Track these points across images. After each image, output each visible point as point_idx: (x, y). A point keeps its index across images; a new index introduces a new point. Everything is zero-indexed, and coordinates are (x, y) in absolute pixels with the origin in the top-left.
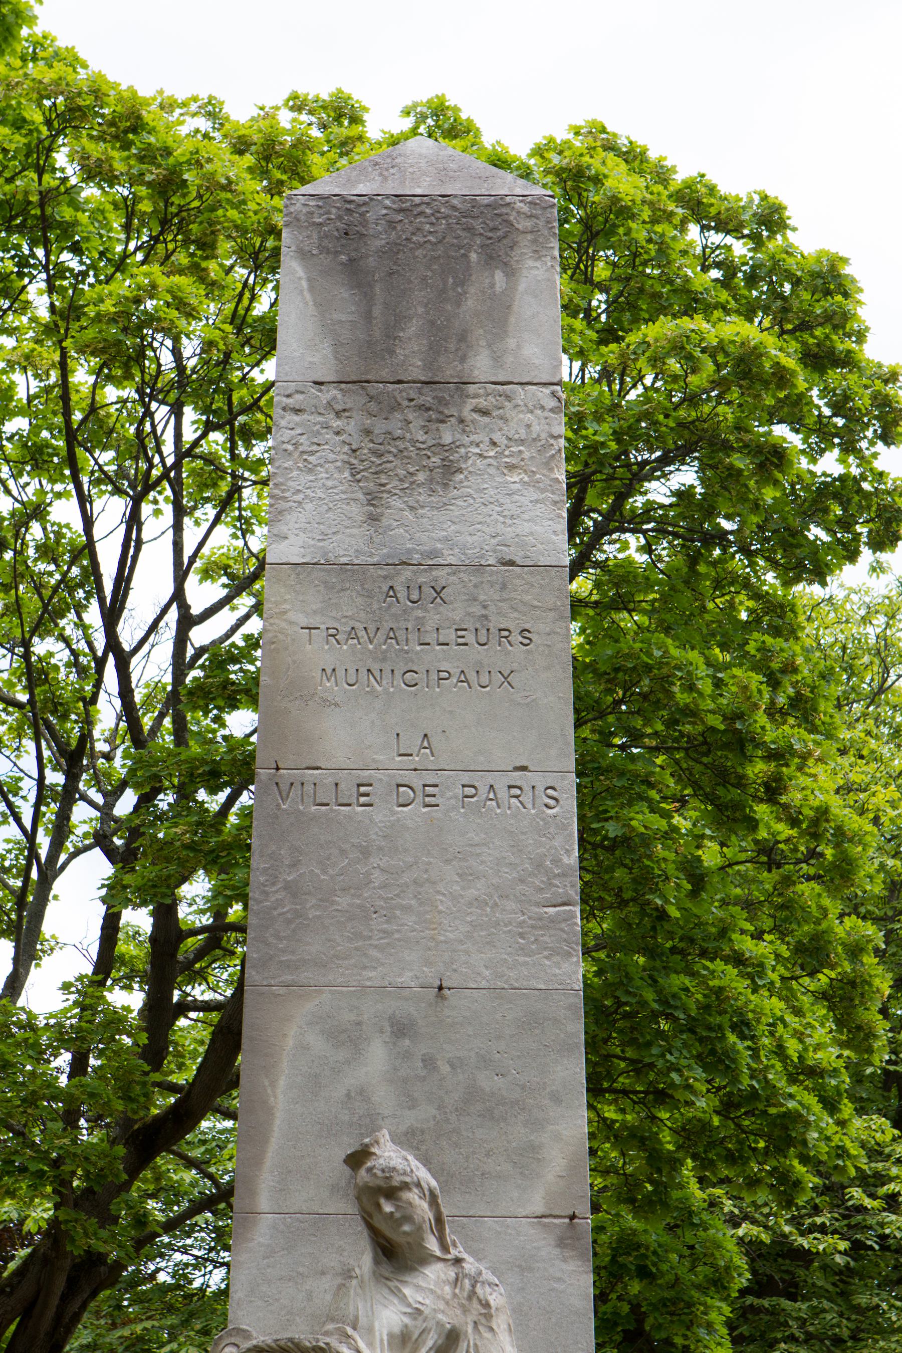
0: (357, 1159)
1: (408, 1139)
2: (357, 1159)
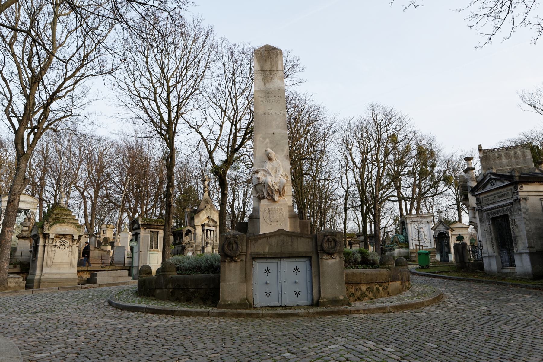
0: (266, 151)
1: (271, 148)
2: (266, 151)
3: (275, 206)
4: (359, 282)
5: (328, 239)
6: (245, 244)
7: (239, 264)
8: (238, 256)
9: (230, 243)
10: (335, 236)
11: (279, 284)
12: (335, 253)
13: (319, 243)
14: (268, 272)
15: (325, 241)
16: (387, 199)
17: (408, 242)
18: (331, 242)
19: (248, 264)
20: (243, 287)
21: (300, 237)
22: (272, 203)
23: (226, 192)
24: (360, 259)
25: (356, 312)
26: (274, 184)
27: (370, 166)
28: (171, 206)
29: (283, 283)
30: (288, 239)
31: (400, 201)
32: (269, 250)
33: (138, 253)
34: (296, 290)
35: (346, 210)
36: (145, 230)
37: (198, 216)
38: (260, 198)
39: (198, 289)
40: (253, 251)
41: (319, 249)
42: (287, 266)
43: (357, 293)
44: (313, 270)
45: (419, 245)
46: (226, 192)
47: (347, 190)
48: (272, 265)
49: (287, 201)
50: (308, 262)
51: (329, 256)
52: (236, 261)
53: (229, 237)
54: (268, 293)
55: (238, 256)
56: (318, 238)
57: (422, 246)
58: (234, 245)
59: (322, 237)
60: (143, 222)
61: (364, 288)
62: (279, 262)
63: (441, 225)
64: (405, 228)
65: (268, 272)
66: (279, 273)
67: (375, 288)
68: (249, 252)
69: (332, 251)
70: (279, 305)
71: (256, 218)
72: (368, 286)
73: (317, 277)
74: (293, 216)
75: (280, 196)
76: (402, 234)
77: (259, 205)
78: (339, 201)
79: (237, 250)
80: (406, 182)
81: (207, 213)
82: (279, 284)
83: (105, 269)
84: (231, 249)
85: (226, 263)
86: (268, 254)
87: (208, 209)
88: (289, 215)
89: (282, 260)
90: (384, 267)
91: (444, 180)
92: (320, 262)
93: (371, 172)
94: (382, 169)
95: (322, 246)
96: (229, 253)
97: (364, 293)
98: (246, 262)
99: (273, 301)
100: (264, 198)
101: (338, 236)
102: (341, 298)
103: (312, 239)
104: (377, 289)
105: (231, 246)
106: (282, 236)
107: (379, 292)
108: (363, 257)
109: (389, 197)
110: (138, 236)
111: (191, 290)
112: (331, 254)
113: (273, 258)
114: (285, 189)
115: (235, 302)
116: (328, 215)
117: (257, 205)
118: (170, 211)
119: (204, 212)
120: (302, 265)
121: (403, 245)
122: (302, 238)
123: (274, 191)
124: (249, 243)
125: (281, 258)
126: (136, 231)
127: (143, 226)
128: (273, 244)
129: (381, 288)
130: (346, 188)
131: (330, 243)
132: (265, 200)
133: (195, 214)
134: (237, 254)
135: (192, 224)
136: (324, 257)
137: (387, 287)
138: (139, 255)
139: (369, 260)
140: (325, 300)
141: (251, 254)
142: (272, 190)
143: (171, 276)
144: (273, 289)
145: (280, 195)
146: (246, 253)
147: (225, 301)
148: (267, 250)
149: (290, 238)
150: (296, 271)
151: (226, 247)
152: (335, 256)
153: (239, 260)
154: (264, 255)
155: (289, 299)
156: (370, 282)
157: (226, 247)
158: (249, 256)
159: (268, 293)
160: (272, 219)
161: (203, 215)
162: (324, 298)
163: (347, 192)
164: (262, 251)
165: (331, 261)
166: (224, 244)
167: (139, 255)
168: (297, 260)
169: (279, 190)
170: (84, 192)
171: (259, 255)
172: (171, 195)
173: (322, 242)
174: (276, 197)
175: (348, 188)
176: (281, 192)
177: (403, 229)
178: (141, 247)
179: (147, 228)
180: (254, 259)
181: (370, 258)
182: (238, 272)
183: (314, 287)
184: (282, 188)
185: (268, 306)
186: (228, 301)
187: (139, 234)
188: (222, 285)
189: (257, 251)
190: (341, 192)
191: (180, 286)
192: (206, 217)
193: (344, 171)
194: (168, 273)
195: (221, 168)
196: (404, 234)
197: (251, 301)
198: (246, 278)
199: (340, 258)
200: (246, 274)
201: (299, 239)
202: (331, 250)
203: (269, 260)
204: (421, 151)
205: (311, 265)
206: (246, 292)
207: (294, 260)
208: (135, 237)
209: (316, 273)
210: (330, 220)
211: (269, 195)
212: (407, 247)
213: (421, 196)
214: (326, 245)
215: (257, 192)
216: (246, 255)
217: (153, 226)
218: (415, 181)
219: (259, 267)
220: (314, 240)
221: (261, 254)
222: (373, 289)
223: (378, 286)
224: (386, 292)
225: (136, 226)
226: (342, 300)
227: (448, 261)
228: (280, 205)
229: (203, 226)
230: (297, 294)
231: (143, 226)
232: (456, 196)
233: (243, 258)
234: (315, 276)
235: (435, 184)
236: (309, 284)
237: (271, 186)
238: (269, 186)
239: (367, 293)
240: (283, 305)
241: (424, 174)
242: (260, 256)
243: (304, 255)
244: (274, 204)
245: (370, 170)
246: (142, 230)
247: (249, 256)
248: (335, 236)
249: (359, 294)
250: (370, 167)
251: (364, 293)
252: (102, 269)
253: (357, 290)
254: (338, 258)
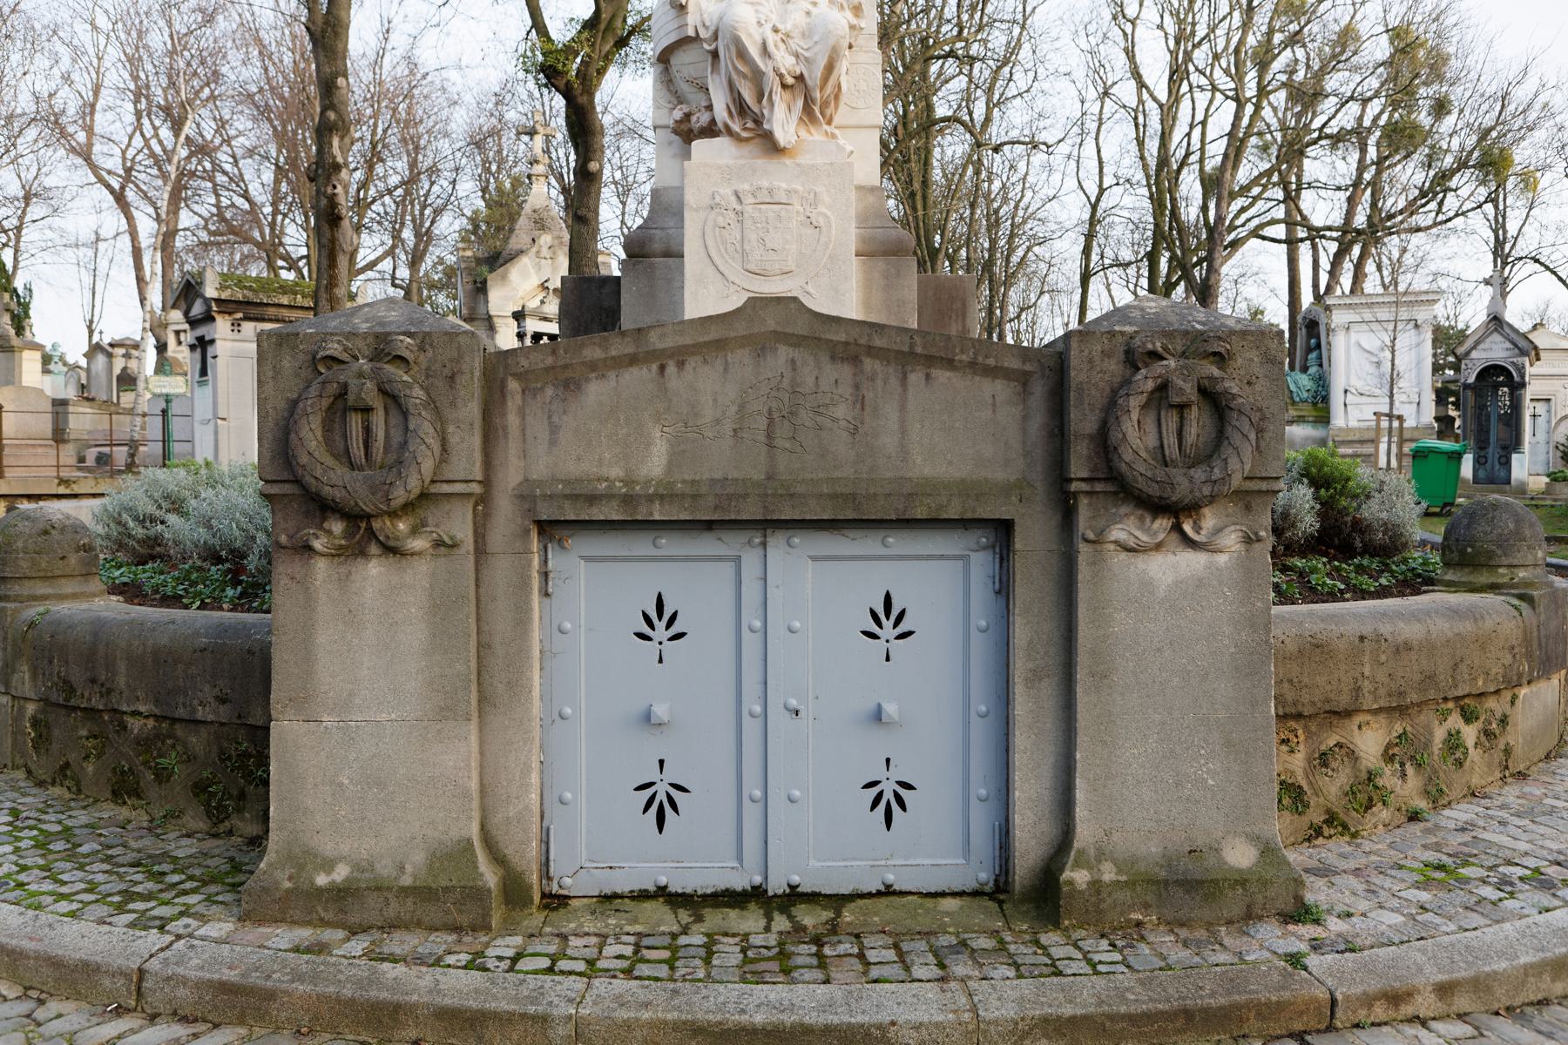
3: (776, 176)
4: (1344, 701)
5: (1163, 387)
6: (471, 409)
7: (419, 573)
8: (408, 507)
9: (341, 405)
10: (1220, 358)
11: (751, 728)
12: (1212, 499)
13: (1083, 421)
14: (661, 632)
15: (1135, 403)
16: (1255, 233)
17: (1326, 399)
18: (1182, 408)
19: (501, 570)
20: (458, 755)
21: (930, 361)
22: (761, 163)
23: (593, 166)
24: (1308, 523)
25: (1380, 1011)
26: (772, 39)
27: (1202, 99)
28: (340, 218)
29: (777, 716)
30: (834, 377)
31: (1291, 243)
32: (671, 465)
33: (211, 426)
34: (878, 773)
35: (1085, 278)
36: (236, 325)
37: (504, 277)
38: (686, 133)
39: (174, 720)
40: (541, 468)
41: (1078, 468)
42: (815, 590)
43: (1323, 781)
44: (1021, 633)
45: (1390, 416)
46: (593, 166)
47: (1098, 199)
48: (697, 580)
49: (846, 152)
50: (982, 565)
51: (1163, 524)
52: (392, 550)
53: (334, 348)
54: (662, 790)
55: (408, 507)
56: (1078, 373)
57: (1400, 418)
58: (378, 420)
59: (1114, 367)
60: (222, 288)
61: (1370, 741)
62: (751, 560)
63: (1496, 337)
64: (1318, 346)
65: (661, 632)
66: (751, 643)
67: (1439, 734)
68: (511, 475)
69: (1183, 485)
70: (740, 883)
71: (667, 254)
72: (1398, 728)
73: (1049, 689)
74: (876, 251)
75: (809, 114)
76: (1305, 369)
77: (683, 176)
78: (1058, 245)
79: (399, 461)
80: (1326, 168)
81: (539, 268)
82: (751, 728)
83: (76, 489)
84: (357, 451)
85: (321, 566)
86: (666, 495)
87: (545, 252)
88: (863, 240)
89: (778, 546)
90: (1484, 578)
91: (1480, 165)
92: (1084, 572)
93: (1204, 123)
94: (1249, 109)
95: (1104, 444)
96: (334, 478)
97: (1371, 776)
98: (481, 551)
99: (699, 857)
100: (710, 131)
101: (1247, 359)
102: (1240, 856)
103: (1023, 380)
104: (1453, 743)
105: (355, 422)
106: (784, 352)
107: (1459, 763)
108: (1327, 510)
109: (1262, 226)
110: (210, 351)
111: (135, 724)
112: (1173, 510)
113: (709, 526)
114: (843, 66)
115: (385, 869)
116: (1014, 296)
117: (670, 180)
118: (333, 241)
119: (525, 261)
120: (937, 584)
121: (1307, 410)
122: (942, 375)
123: (772, 82)
124: (514, 402)
125: (768, 525)
126: (200, 332)
127: (227, 306)
128: (709, 413)
129: (1470, 733)
130: (1093, 191)
131: (1171, 421)
132: (721, 142)
133: (492, 270)
134: (399, 496)
135: (481, 310)
136: (1117, 533)
137: (1504, 721)
138: (216, 433)
139: (1358, 526)
140: (1108, 874)
141: (526, 496)
142: (757, 77)
143: (32, 612)
144: (702, 765)
145: (808, 109)
146: (486, 482)
147: (306, 859)
148: (655, 464)
149: (846, 371)
150: (888, 630)
151: (311, 435)
152: (1209, 519)
153: (418, 544)
154: (628, 500)
155: (824, 845)
156: (1414, 697)
157: (311, 435)
158: (505, 510)
159: (662, 790)
160: (756, 257)
161: (525, 275)
162: (1101, 855)
163: (1094, 207)
164: (616, 472)
165: (1171, 567)
166: (293, 404)
167: (216, 433)
168: (897, 542)
169: (800, 78)
170: (123, 188)
171: (592, 499)
172: (337, 168)
173: (1111, 408)
174: (783, 121)
175: (1102, 191)
176: (814, 100)
177: (1309, 350)
178: (221, 399)
179: (247, 318)
180: (549, 529)
181: (1372, 511)
182: (414, 634)
183: (1018, 759)
184: (822, 63)
185: (662, 893)
186: (329, 865)
187: (212, 341)
188: (286, 732)
189: (572, 469)
190: (1073, 210)
191: (70, 689)
192: (535, 281)
193: (1089, 129)
194: (25, 589)
195: (569, 50)
196: (1313, 370)
197: (527, 858)
198: (484, 679)
199: (1249, 540)
200: (483, 647)
201: (916, 377)
202: (1178, 475)
203: (669, 544)
204: (1404, 42)
205: (1004, 589)
207: (867, 543)
208: (198, 354)
209: (1047, 657)
210: (1018, 317)
211: (741, 108)
212: (1324, 418)
213: (1374, 233)
214: (1138, 436)
215: (680, 100)
216: (483, 501)
217: (272, 311)
218: (1361, 168)
219: (590, 600)
220: (1039, 390)
221: (609, 496)
222: (1427, 745)
223: (1455, 721)
224: (1498, 756)
225: (197, 309)
226: (1241, 880)
227: (1508, 482)
229: (519, 316)
230: (889, 804)
231: (227, 306)
232: (1495, 232)
233: (459, 525)
234: (1034, 677)
235: (1439, 185)
236: (982, 735)
237: (754, 52)
238: (742, 53)
239: (1389, 778)
240: (776, 886)
241: (1401, 138)
242: (598, 513)
243: (952, 514)
245: (1199, 117)
246: (222, 326)
247: (505, 510)
248: (1220, 358)
249: (1334, 785)
250: (1202, 99)
251: (1371, 776)
252: (62, 490)
253: (1324, 759)
254: (1231, 539)
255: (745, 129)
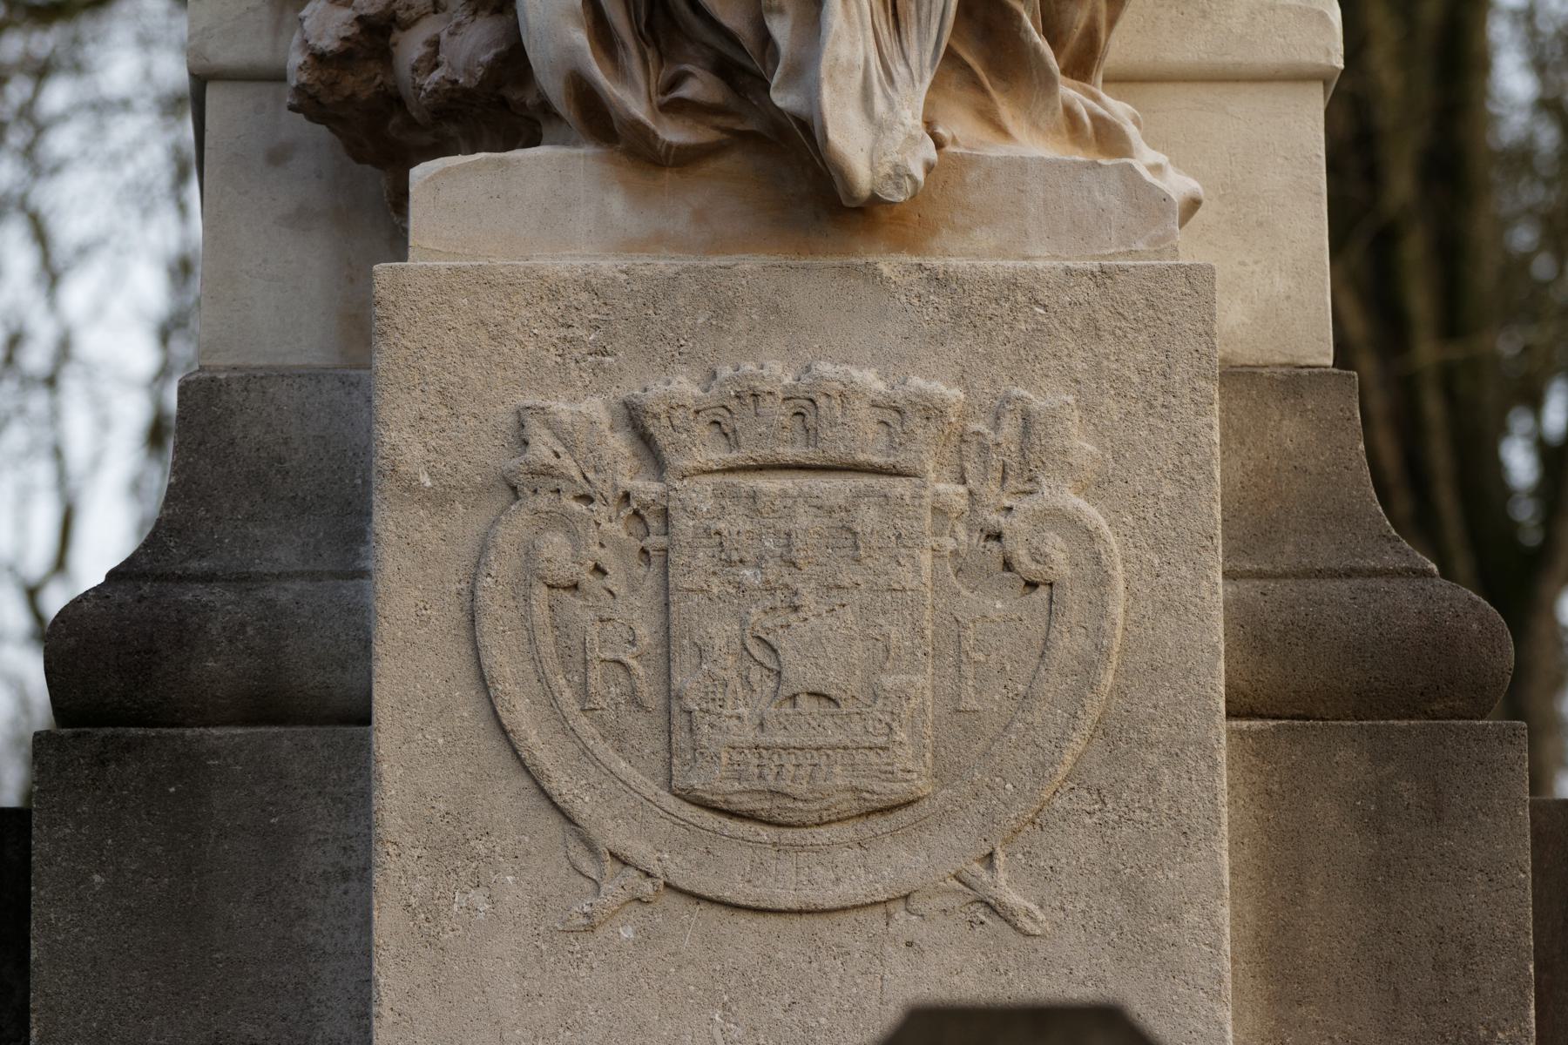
3: (848, 341)
77: (358, 324)
100: (500, 109)
117: (282, 329)
132: (549, 168)
206: (1296, 576)
228: (966, 308)
244: (809, 282)
255: (675, 108)
